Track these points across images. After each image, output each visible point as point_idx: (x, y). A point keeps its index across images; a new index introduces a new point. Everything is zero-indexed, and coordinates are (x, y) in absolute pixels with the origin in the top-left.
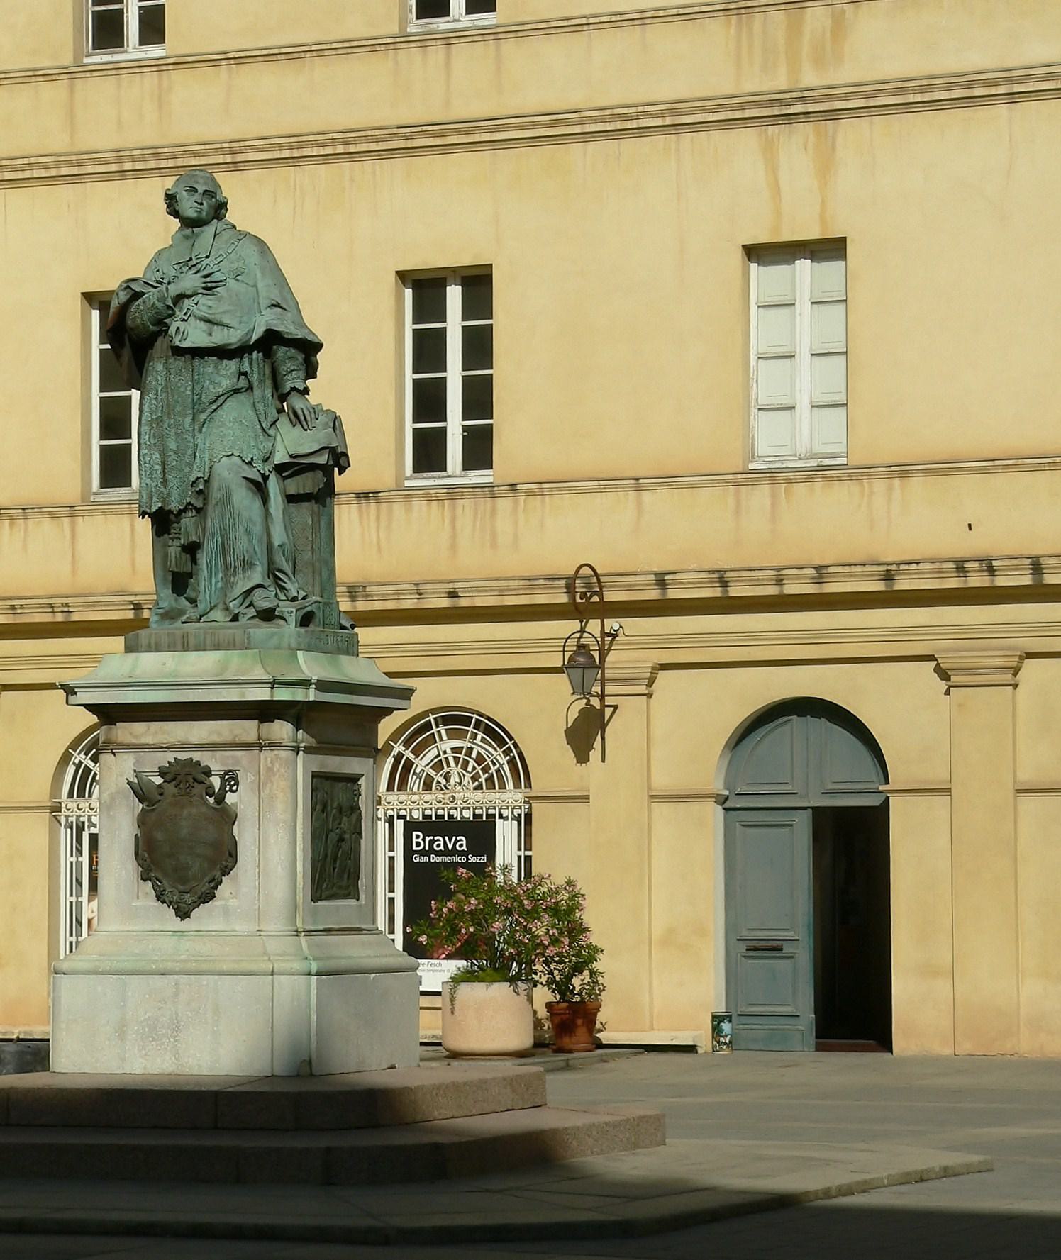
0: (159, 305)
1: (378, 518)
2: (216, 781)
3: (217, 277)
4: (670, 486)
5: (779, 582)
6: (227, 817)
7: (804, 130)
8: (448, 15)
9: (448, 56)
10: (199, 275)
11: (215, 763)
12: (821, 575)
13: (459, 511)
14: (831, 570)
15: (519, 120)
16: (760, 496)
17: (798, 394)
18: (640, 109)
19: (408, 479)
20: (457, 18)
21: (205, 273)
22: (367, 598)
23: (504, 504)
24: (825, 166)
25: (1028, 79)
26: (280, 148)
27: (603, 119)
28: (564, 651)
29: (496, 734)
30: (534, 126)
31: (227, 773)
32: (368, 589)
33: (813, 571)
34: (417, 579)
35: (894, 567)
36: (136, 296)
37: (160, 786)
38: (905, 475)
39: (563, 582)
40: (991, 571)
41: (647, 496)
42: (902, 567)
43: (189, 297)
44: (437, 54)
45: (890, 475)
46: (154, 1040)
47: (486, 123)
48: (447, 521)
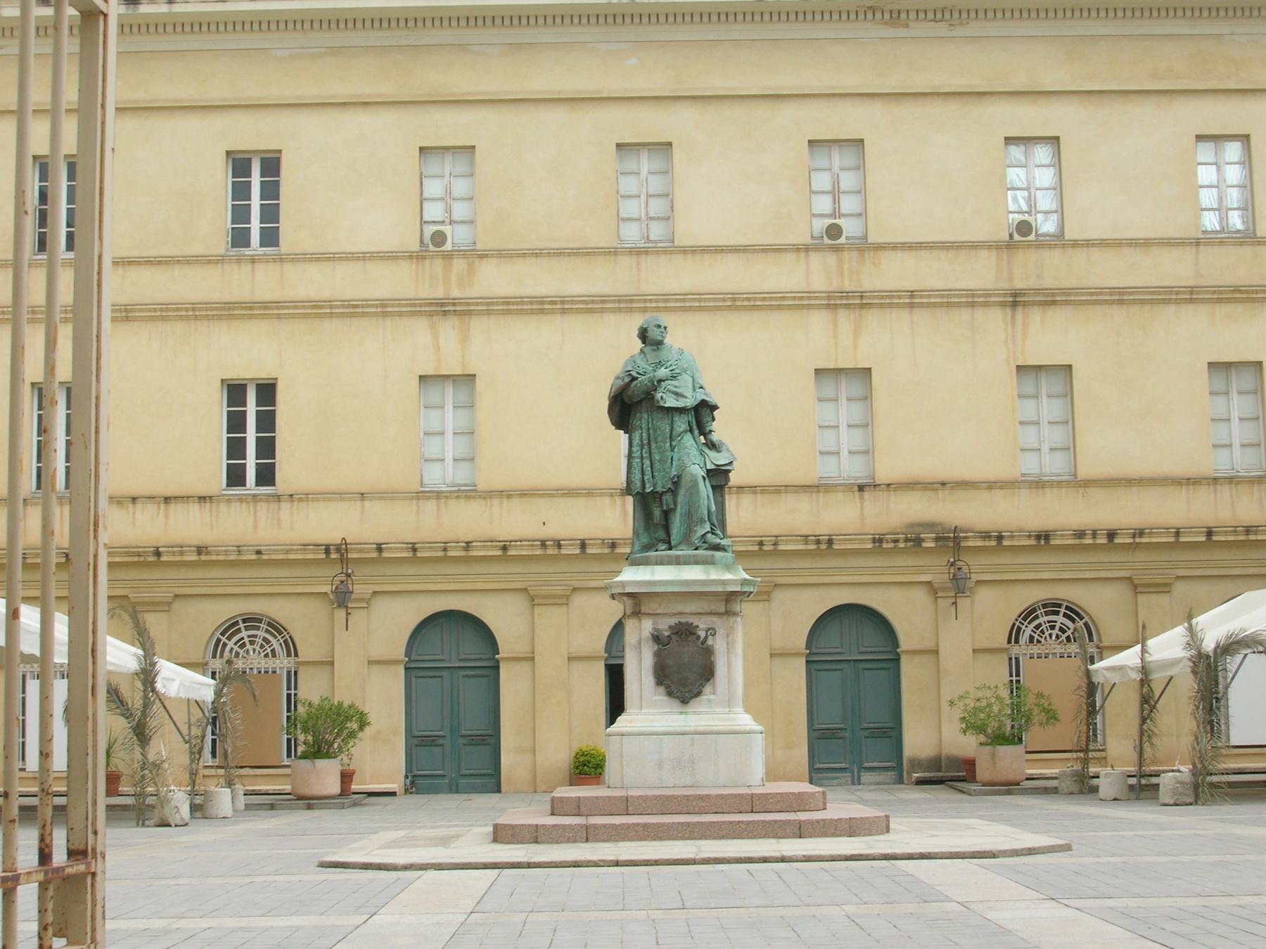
0: (649, 384)
1: (211, 510)
2: (702, 634)
3: (677, 371)
4: (381, 498)
5: (445, 549)
6: (708, 652)
7: (453, 321)
8: (249, 247)
9: (253, 268)
10: (668, 370)
11: (702, 624)
12: (468, 547)
13: (259, 508)
14: (474, 544)
15: (295, 304)
16: (430, 506)
17: (446, 454)
18: (364, 303)
19: (224, 490)
20: (255, 248)
21: (671, 368)
22: (208, 553)
23: (285, 506)
24: (465, 338)
25: (572, 302)
26: (801, 298)
27: (343, 306)
28: (332, 584)
29: (276, 627)
30: (304, 307)
31: (709, 629)
32: (209, 549)
33: (464, 544)
34: (238, 544)
35: (508, 543)
36: (634, 379)
37: (668, 636)
38: (509, 497)
39: (324, 547)
40: (559, 546)
41: (367, 503)
42: (513, 543)
43: (664, 381)
44: (246, 268)
45: (501, 497)
46: (680, 769)
47: (277, 304)
48: (252, 513)
